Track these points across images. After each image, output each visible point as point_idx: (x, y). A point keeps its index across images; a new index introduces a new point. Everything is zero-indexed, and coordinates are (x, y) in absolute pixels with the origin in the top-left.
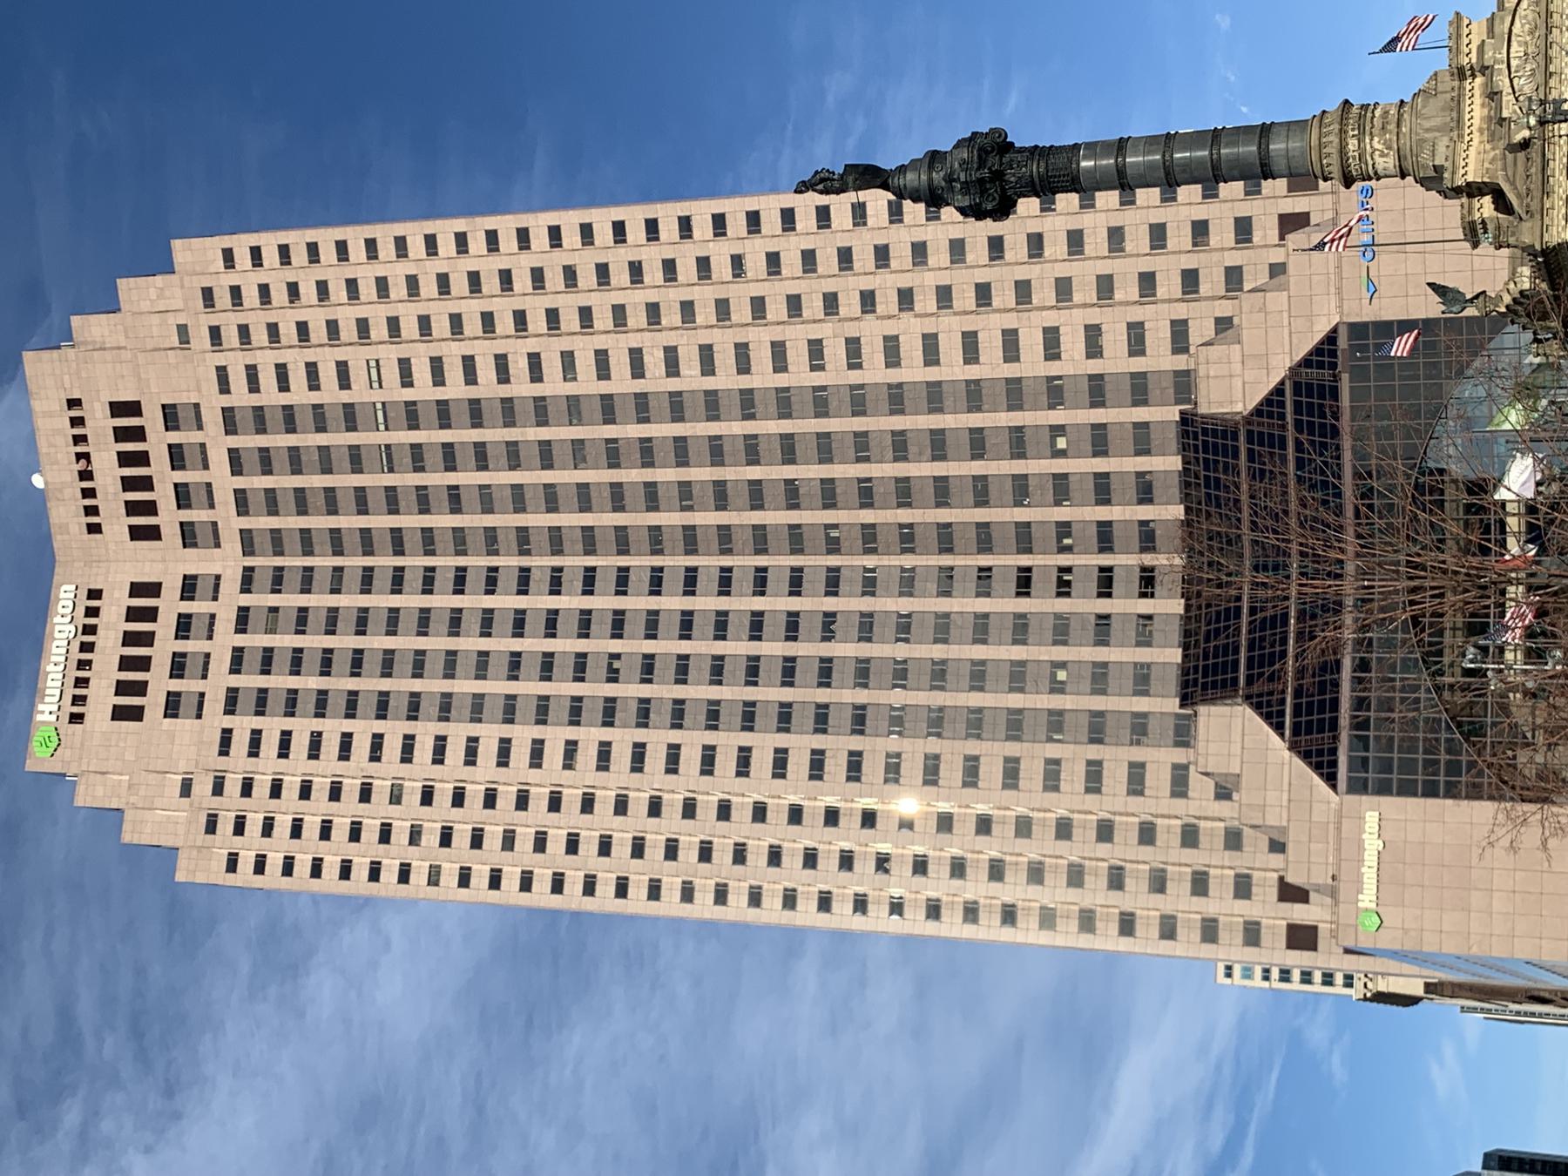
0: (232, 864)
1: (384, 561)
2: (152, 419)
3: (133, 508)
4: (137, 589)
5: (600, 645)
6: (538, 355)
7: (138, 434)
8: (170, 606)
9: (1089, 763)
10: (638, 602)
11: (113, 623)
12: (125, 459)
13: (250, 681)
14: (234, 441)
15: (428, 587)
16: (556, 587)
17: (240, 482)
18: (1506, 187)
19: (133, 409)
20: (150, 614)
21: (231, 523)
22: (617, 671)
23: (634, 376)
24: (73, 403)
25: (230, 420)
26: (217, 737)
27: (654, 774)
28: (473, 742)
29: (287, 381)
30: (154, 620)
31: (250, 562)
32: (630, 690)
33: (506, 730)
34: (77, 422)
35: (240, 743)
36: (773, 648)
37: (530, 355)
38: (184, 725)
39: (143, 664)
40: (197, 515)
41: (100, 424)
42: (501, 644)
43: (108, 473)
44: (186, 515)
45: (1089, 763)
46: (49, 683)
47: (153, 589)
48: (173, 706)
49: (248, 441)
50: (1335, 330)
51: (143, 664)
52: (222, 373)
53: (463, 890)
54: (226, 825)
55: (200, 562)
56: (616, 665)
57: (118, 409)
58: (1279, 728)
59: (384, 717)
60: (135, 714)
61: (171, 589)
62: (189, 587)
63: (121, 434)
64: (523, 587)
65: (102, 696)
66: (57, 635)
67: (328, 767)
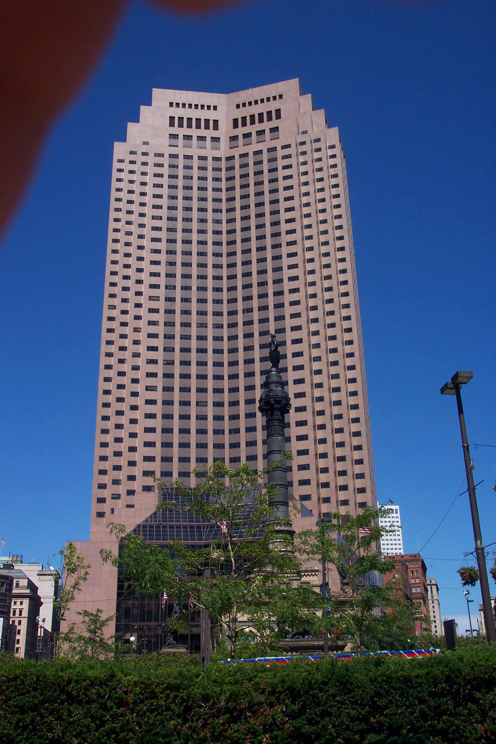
1: (223, 175)
2: (274, 123)
3: (244, 119)
4: (216, 122)
5: (195, 248)
6: (297, 255)
8: (209, 133)
10: (210, 319)
11: (204, 115)
12: (261, 115)
13: (181, 162)
14: (265, 152)
15: (215, 232)
16: (215, 278)
17: (251, 154)
19: (278, 117)
21: (236, 153)
23: (294, 380)
24: (281, 97)
25: (272, 150)
27: (147, 342)
28: (162, 165)
29: (286, 169)
31: (223, 159)
32: (179, 236)
33: (163, 275)
34: (275, 98)
35: (159, 160)
36: (194, 357)
37: (296, 253)
38: (167, 141)
39: (190, 126)
40: (241, 140)
41: (273, 106)
42: (195, 204)
43: (256, 110)
44: (241, 137)
47: (216, 127)
49: (265, 157)
51: (190, 126)
52: (288, 146)
54: (133, 158)
55: (224, 143)
57: (278, 111)
59: (168, 209)
60: (172, 124)
61: (216, 134)
62: (216, 140)
64: (216, 339)
65: (178, 113)
67: (150, 170)
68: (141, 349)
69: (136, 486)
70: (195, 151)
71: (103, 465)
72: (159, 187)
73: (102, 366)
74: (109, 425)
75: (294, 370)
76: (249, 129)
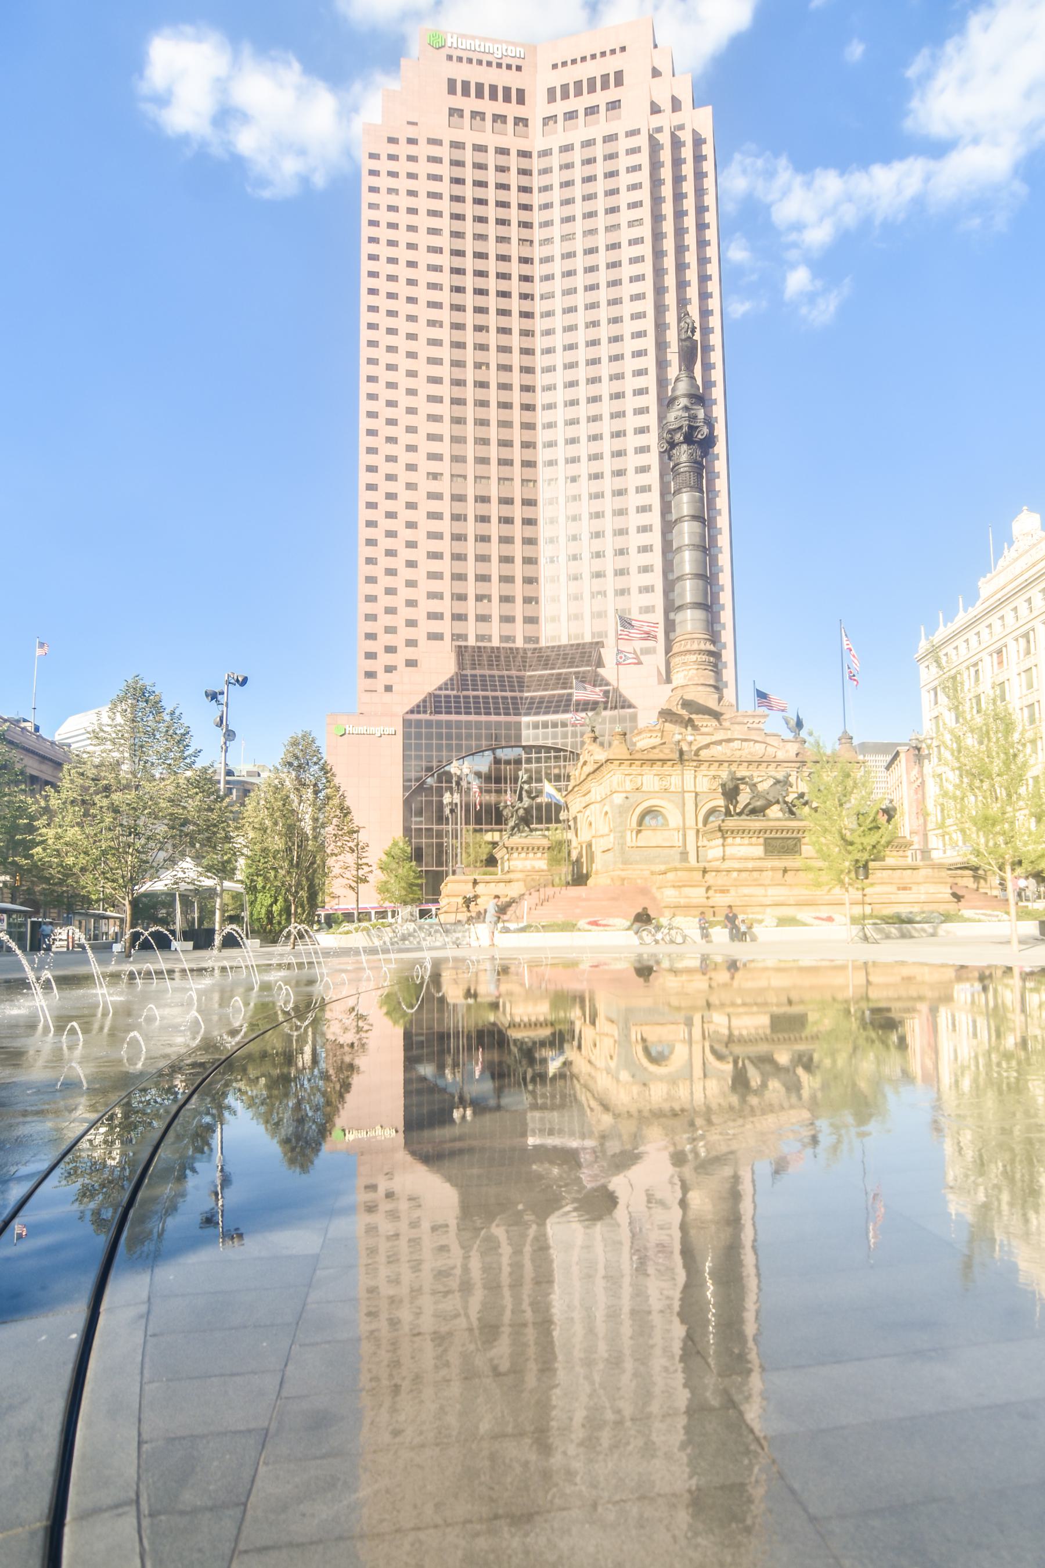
0: (373, 156)
2: (613, 93)
3: (565, 88)
4: (521, 93)
8: (512, 110)
9: (442, 614)
11: (502, 78)
18: (645, 1062)
20: (507, 99)
22: (480, 368)
24: (623, 49)
26: (410, 126)
30: (483, 85)
34: (613, 52)
41: (610, 65)
45: (442, 614)
47: (521, 101)
50: (634, 707)
53: (366, 291)
54: (393, 149)
56: (484, 368)
60: (452, 90)
61: (520, 111)
63: (605, 77)
65: (463, 73)
68: (418, 516)
69: (419, 634)
70: (491, 139)
71: (370, 646)
72: (436, 252)
73: (362, 487)
74: (377, 571)
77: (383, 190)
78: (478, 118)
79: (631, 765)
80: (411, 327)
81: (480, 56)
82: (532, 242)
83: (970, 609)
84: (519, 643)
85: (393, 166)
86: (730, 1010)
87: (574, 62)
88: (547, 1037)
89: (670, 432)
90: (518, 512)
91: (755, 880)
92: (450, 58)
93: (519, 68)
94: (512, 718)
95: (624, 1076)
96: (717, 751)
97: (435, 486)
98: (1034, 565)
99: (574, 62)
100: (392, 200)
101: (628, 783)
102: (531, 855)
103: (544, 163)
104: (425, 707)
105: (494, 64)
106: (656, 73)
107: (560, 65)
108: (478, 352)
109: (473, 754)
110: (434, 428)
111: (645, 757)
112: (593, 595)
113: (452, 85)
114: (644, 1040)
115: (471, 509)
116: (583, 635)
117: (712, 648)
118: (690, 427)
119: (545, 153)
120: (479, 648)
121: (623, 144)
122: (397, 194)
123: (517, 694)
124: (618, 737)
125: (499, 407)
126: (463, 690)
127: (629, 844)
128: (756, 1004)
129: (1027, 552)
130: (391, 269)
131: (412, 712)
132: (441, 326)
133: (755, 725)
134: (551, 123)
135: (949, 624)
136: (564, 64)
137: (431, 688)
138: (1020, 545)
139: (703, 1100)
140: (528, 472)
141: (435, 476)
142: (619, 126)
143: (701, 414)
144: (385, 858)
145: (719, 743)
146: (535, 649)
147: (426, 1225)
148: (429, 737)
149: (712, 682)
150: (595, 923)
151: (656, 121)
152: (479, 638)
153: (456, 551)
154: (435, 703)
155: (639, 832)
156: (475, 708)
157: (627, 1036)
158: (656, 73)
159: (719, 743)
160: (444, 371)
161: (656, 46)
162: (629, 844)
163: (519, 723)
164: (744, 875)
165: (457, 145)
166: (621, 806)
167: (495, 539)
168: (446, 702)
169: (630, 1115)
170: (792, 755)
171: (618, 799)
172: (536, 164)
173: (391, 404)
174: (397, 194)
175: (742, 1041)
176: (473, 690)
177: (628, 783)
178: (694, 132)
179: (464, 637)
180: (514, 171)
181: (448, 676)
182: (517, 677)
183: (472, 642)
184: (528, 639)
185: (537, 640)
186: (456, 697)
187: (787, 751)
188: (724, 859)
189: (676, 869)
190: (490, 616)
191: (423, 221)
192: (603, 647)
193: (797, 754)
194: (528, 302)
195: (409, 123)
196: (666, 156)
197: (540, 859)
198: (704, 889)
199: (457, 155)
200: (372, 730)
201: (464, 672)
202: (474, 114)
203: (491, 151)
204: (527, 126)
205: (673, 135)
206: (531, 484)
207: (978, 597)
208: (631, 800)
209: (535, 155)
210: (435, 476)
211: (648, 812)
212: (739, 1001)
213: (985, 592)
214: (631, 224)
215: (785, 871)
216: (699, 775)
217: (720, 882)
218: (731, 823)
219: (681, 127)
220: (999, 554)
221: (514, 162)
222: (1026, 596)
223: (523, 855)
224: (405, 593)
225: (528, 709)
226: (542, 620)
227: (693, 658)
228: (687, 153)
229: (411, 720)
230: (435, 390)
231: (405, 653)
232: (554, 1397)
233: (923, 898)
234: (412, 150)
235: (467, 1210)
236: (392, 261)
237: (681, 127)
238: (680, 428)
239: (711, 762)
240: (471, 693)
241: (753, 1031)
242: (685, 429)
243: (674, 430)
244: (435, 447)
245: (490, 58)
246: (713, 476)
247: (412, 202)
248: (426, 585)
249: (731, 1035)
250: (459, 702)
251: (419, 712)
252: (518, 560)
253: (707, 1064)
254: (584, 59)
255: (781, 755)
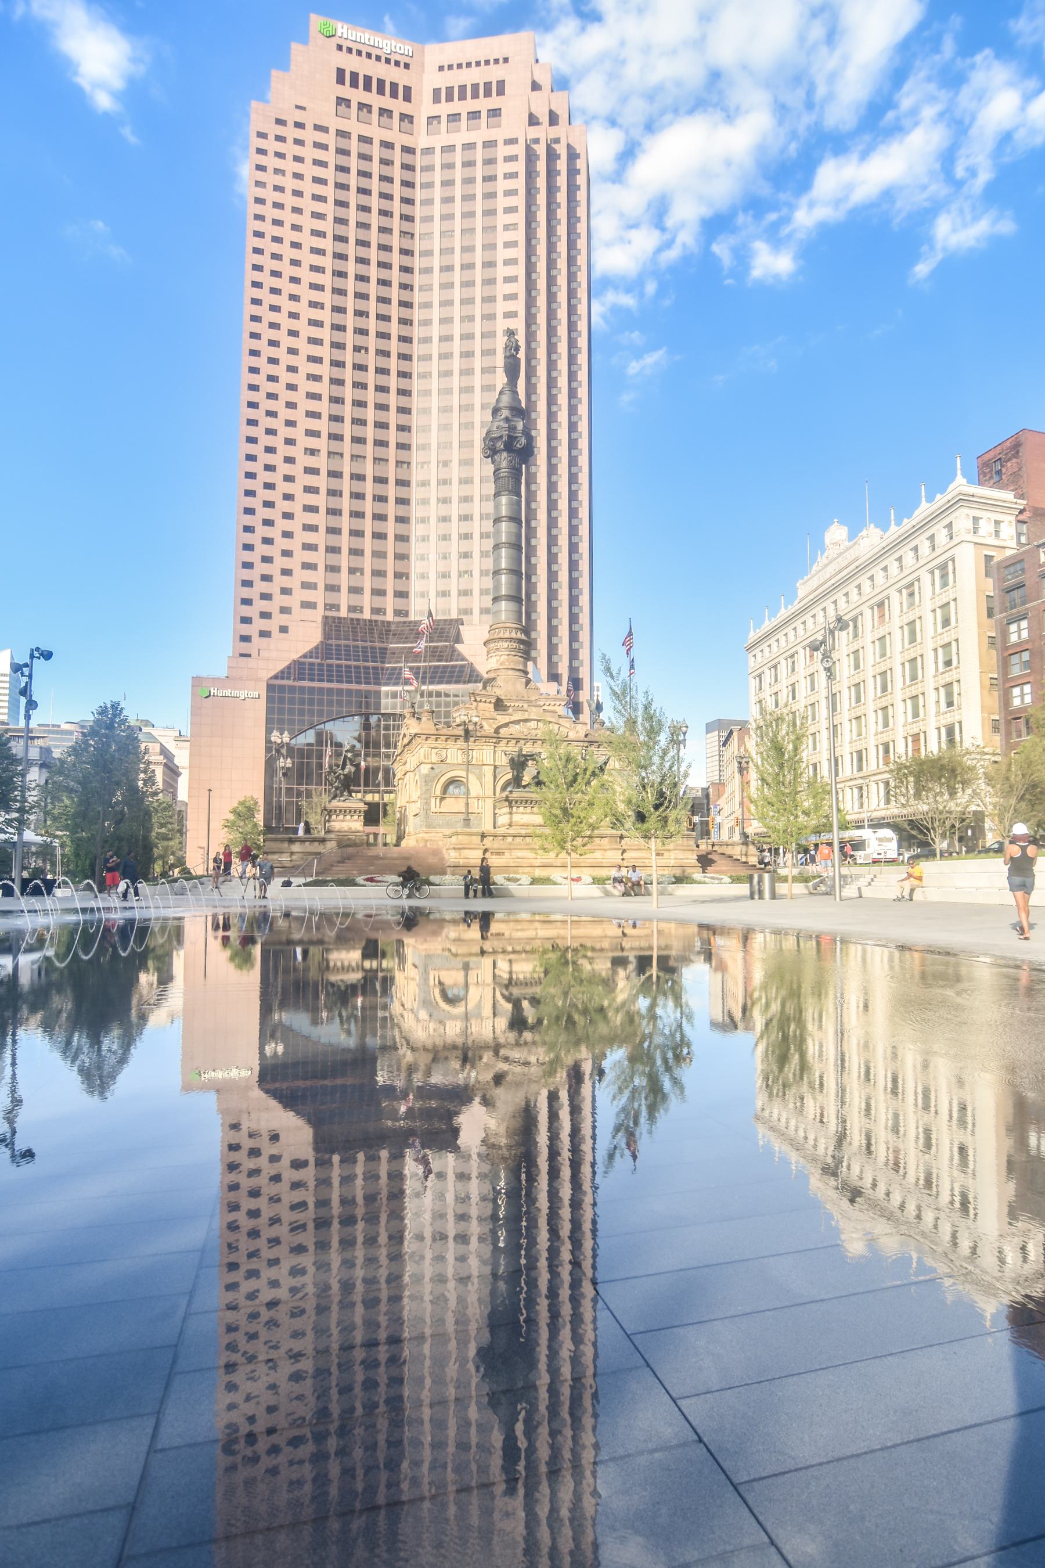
0: (262, 135)
2: (494, 102)
3: (450, 90)
4: (407, 90)
7: (488, 94)
8: (398, 106)
11: (390, 74)
12: (475, 87)
19: (501, 92)
20: (394, 95)
24: (506, 60)
25: (490, 144)
34: (496, 61)
41: (494, 73)
46: (359, 34)
47: (407, 98)
48: (341, 101)
51: (367, 87)
54: (280, 130)
56: (363, 351)
57: (501, 84)
58: (305, 656)
60: (340, 80)
65: (352, 64)
66: (385, 42)
72: (319, 236)
75: (505, 178)
76: (456, 106)
77: (270, 170)
78: (365, 110)
79: (436, 739)
80: (293, 307)
81: (370, 50)
82: (413, 235)
83: (790, 607)
84: (390, 617)
85: (280, 147)
86: (512, 956)
87: (460, 66)
88: (359, 981)
89: (493, 440)
90: (391, 491)
91: (528, 844)
92: (340, 48)
93: (407, 66)
94: (372, 687)
95: (423, 1015)
96: (514, 729)
97: (312, 462)
98: (840, 571)
99: (460, 66)
100: (279, 180)
101: (434, 755)
102: (348, 817)
103: (426, 161)
104: (289, 673)
105: (383, 59)
106: (536, 86)
107: (446, 68)
108: (357, 336)
109: (334, 720)
110: (313, 406)
111: (449, 733)
112: (461, 574)
113: (340, 73)
114: (440, 983)
115: (346, 485)
116: (449, 610)
117: (523, 637)
118: (509, 437)
119: (428, 151)
120: (352, 619)
121: (502, 151)
122: (284, 175)
123: (379, 664)
124: (426, 714)
125: (376, 390)
126: (327, 658)
127: (433, 809)
128: (526, 952)
129: (835, 559)
130: (276, 248)
131: (275, 677)
132: (322, 308)
133: (551, 708)
134: (435, 122)
135: (773, 619)
136: (450, 67)
137: (295, 656)
138: (831, 552)
139: (491, 1035)
140: (403, 455)
141: (313, 452)
142: (499, 134)
143: (520, 425)
144: (231, 817)
145: (517, 722)
146: (405, 622)
147: (285, 1162)
148: (292, 701)
149: (521, 667)
150: (371, 880)
151: (534, 132)
152: (352, 609)
153: (331, 525)
154: (298, 669)
155: (442, 799)
156: (337, 676)
157: (426, 980)
158: (536, 86)
159: (517, 722)
160: (324, 352)
161: (537, 61)
162: (433, 809)
163: (378, 694)
164: (518, 840)
165: (342, 134)
166: (426, 775)
167: (369, 515)
168: (309, 669)
169: (425, 1049)
170: (581, 736)
171: (425, 769)
172: (419, 161)
173: (272, 379)
174: (284, 175)
175: (518, 984)
176: (337, 659)
177: (434, 755)
178: (569, 146)
179: (336, 607)
180: (397, 165)
181: (315, 644)
182: (380, 648)
183: (344, 613)
184: (397, 613)
185: (406, 614)
186: (319, 665)
187: (577, 732)
188: (510, 825)
189: (457, 834)
190: (362, 589)
191: (308, 205)
192: (462, 624)
193: (586, 736)
194: (407, 292)
195: (297, 107)
196: (541, 166)
197: (356, 821)
198: (481, 852)
199: (343, 143)
200: (236, 693)
201: (330, 642)
202: (361, 106)
203: (376, 143)
204: (411, 122)
205: (549, 147)
206: (405, 466)
207: (797, 596)
208: (436, 771)
209: (418, 152)
210: (313, 452)
211: (452, 782)
212: (510, 949)
213: (802, 592)
214: (506, 227)
215: (622, 837)
216: (499, 750)
217: (496, 846)
218: (517, 794)
219: (557, 141)
220: (814, 560)
221: (397, 156)
222: (833, 599)
223: (341, 817)
224: (280, 562)
225: (388, 679)
226: (412, 595)
227: (505, 645)
228: (562, 165)
229: (274, 685)
230: (314, 369)
231: (278, 619)
232: (995, 1519)
233: (672, 862)
234: (299, 134)
235: (323, 1145)
236: (277, 240)
237: (557, 141)
238: (501, 437)
239: (509, 739)
240: (335, 662)
241: (528, 976)
242: (505, 438)
243: (496, 438)
244: (313, 424)
245: (379, 53)
246: (531, 479)
247: (298, 185)
248: (301, 556)
249: (511, 979)
250: (322, 670)
251: (282, 678)
252: (391, 537)
253: (497, 1005)
254: (469, 65)
255: (572, 735)
